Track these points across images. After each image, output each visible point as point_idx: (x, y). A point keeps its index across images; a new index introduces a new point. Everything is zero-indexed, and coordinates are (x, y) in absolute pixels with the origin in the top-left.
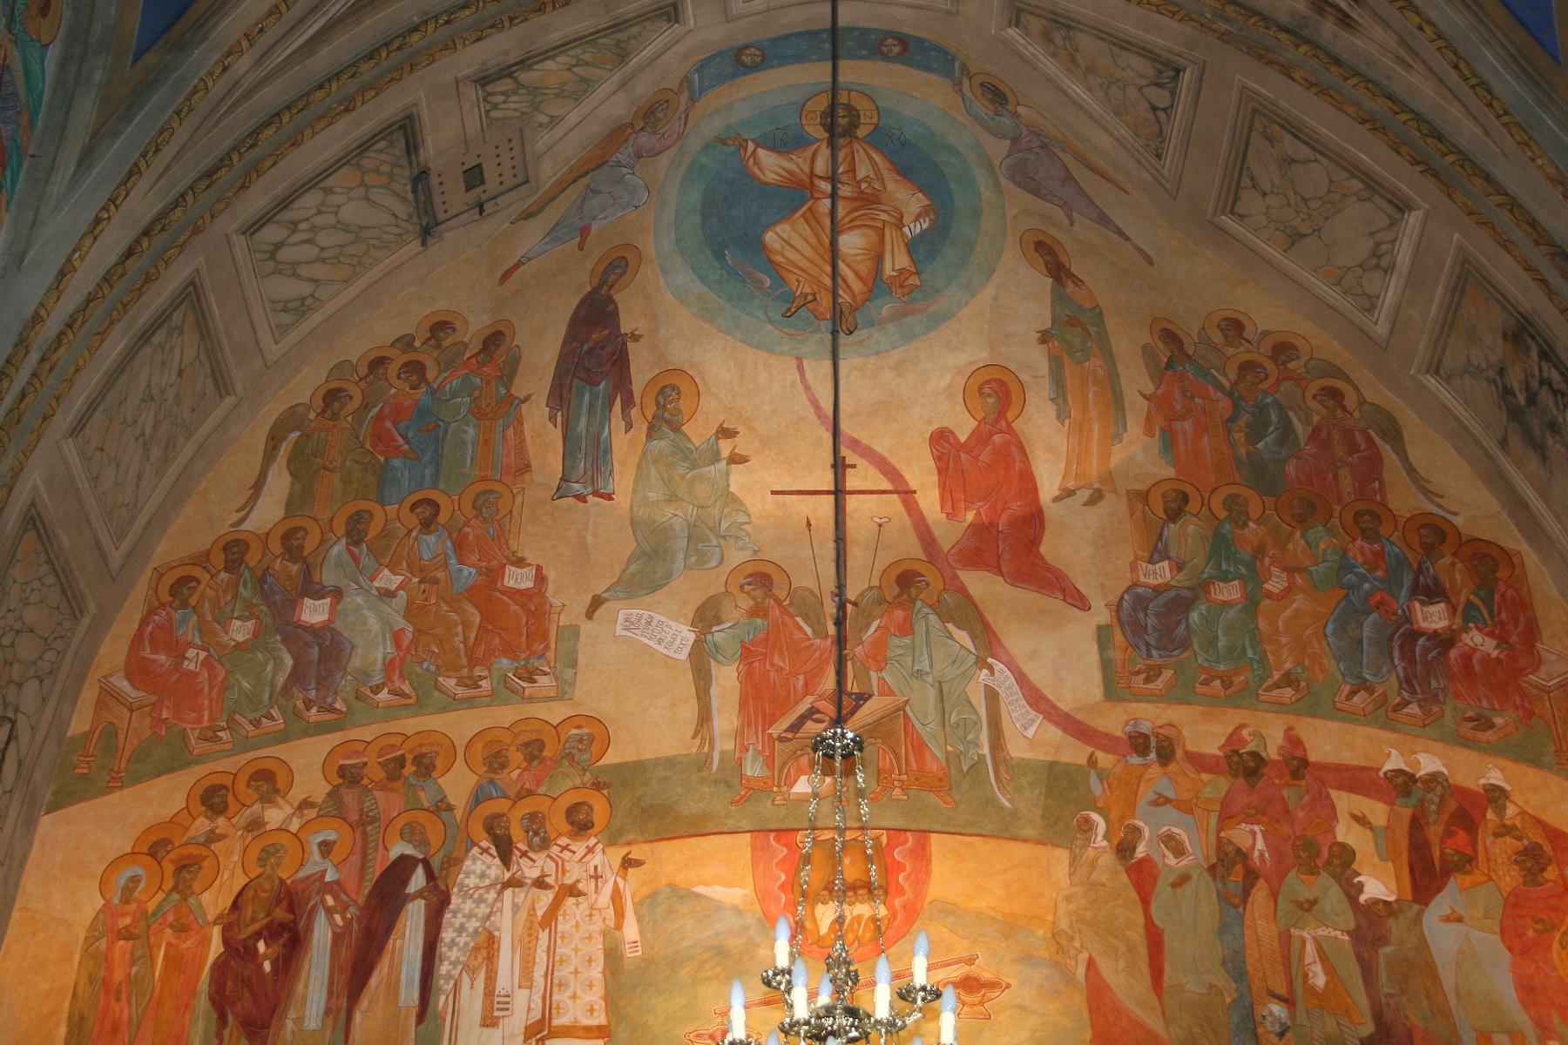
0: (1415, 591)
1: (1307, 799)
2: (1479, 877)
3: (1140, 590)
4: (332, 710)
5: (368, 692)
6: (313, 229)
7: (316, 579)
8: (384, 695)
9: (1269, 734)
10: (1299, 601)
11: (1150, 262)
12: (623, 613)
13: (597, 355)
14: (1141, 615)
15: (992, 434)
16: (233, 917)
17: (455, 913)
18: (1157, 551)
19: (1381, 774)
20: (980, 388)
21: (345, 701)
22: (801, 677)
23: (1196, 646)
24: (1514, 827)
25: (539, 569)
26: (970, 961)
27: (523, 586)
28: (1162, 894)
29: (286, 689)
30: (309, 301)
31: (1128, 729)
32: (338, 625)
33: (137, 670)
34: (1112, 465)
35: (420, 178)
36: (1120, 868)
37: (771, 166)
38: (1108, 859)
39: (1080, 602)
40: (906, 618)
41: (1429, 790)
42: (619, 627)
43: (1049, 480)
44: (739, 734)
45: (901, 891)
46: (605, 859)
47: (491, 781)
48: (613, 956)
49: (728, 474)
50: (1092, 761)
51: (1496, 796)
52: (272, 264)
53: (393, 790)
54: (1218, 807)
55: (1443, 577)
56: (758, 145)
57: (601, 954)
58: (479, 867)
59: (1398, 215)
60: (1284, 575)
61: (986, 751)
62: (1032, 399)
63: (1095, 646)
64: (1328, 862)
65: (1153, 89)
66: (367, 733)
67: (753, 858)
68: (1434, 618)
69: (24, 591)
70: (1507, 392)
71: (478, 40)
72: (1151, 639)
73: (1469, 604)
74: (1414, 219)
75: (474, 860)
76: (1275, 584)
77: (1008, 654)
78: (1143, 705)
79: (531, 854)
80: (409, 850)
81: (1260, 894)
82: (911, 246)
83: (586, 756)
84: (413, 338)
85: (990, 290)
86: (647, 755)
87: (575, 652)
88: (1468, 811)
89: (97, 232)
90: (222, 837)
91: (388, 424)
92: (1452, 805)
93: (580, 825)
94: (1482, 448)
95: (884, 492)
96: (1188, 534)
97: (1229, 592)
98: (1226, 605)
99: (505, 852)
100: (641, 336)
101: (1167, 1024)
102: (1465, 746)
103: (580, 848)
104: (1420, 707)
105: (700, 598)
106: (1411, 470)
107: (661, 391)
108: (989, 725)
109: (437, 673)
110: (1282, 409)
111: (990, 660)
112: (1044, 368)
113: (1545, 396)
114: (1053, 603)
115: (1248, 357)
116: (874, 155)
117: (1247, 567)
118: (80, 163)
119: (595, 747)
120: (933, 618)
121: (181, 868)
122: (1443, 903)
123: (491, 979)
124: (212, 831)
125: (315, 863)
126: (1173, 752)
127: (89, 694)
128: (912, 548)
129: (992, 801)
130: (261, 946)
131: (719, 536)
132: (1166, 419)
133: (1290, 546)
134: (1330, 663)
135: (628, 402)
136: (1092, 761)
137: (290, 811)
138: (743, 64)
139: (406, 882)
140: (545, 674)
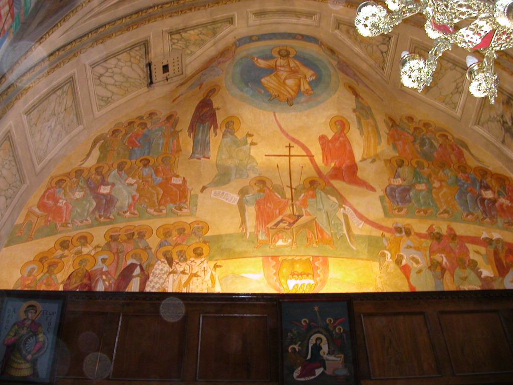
1: (458, 246)
4: (109, 218)
5: (122, 213)
6: (113, 72)
7: (106, 180)
8: (128, 214)
10: (445, 190)
12: (213, 192)
14: (394, 193)
15: (339, 137)
16: (68, 282)
17: (151, 282)
18: (396, 175)
20: (335, 123)
21: (114, 216)
25: (184, 178)
28: (413, 275)
29: (93, 212)
30: (110, 99)
31: (394, 226)
32: (113, 193)
33: (42, 205)
34: (378, 152)
37: (262, 63)
38: (393, 265)
40: (313, 193)
42: (212, 195)
43: (358, 154)
44: (256, 227)
45: (319, 276)
46: (209, 265)
47: (166, 241)
49: (250, 149)
52: (98, 81)
55: (489, 184)
56: (258, 58)
58: (160, 267)
60: (439, 183)
61: (345, 232)
63: (379, 202)
64: (469, 265)
65: (382, 46)
66: (121, 225)
68: (488, 195)
69: (3, 162)
70: (505, 123)
72: (398, 200)
75: (159, 265)
76: (436, 184)
79: (180, 263)
80: (134, 261)
81: (447, 275)
82: (310, 83)
85: (336, 96)
86: (222, 233)
87: (196, 202)
89: (41, 41)
90: (66, 256)
93: (198, 253)
96: (406, 171)
97: (422, 187)
98: (421, 190)
99: (170, 262)
100: (220, 108)
103: (198, 261)
106: (473, 155)
108: (346, 224)
109: (147, 207)
110: (429, 139)
111: (344, 206)
112: (355, 118)
114: (364, 189)
116: (295, 61)
118: (38, 25)
120: (323, 194)
121: (50, 266)
124: (63, 254)
125: (99, 265)
128: (314, 174)
129: (349, 247)
131: (246, 170)
132: (394, 139)
134: (458, 206)
135: (216, 127)
137: (91, 248)
139: (133, 272)
140: (186, 208)
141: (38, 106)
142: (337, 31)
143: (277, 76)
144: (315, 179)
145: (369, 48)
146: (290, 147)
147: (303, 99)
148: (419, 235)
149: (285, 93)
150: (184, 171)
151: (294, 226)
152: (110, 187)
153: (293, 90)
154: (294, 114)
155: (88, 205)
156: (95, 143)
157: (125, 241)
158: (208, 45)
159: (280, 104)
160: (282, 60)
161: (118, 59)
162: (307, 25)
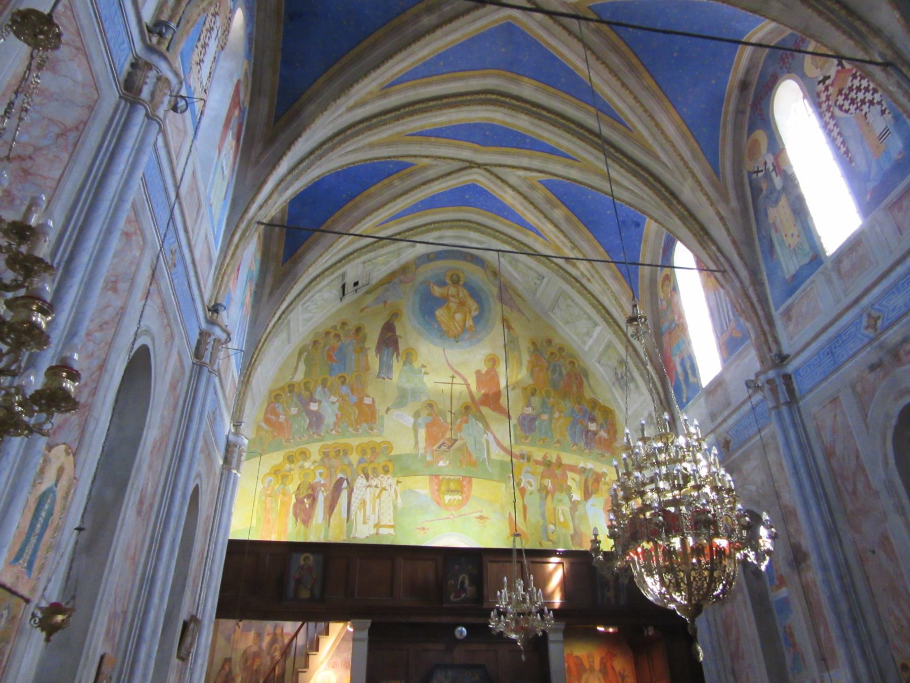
8: (334, 432)
10: (562, 420)
12: (394, 412)
13: (389, 340)
18: (529, 404)
28: (527, 496)
32: (321, 411)
37: (437, 291)
44: (425, 448)
46: (393, 481)
66: (330, 443)
74: (598, 329)
80: (342, 476)
93: (386, 472)
96: (536, 401)
97: (545, 417)
103: (386, 477)
122: (591, 501)
123: (365, 511)
128: (468, 400)
134: (568, 438)
143: (448, 308)
147: (467, 336)
148: (537, 462)
150: (377, 393)
156: (300, 354)
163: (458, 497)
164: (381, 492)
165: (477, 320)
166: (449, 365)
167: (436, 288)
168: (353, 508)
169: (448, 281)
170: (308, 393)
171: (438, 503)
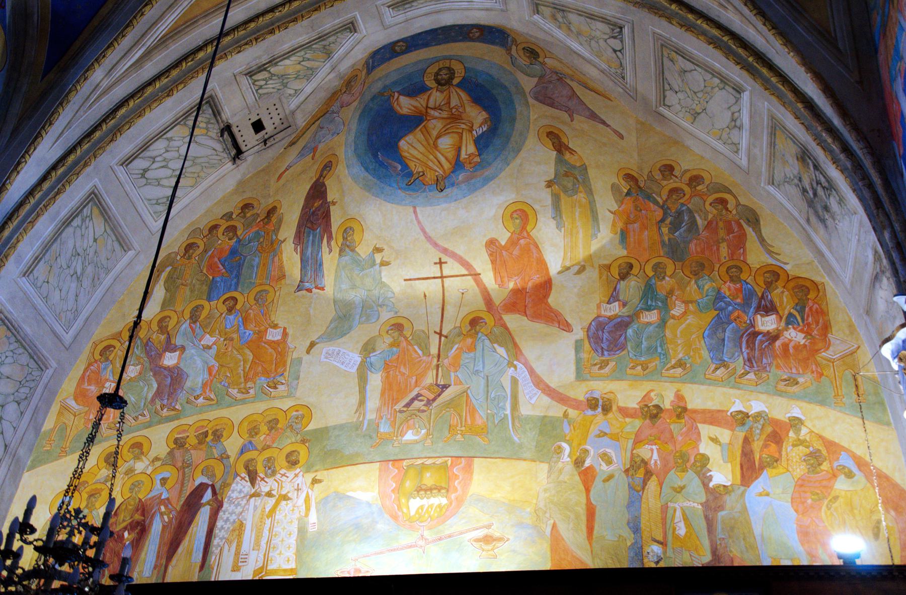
0: (758, 309)
2: (781, 470)
3: (601, 319)
4: (174, 409)
6: (165, 160)
7: (173, 342)
9: (665, 394)
10: (690, 319)
11: (621, 137)
13: (316, 216)
14: (600, 333)
15: (519, 239)
18: (613, 297)
19: (729, 414)
20: (511, 215)
21: (181, 404)
22: (414, 378)
23: (629, 348)
24: (805, 441)
25: (285, 329)
26: (489, 527)
27: (276, 339)
28: (597, 485)
31: (587, 396)
32: (182, 365)
34: (592, 251)
35: (227, 129)
36: (576, 473)
37: (405, 105)
39: (566, 327)
41: (756, 421)
42: (322, 357)
43: (554, 263)
44: (379, 410)
45: (456, 490)
46: (304, 479)
47: (250, 442)
48: (302, 531)
49: (380, 272)
50: (566, 415)
51: (796, 423)
52: (144, 180)
53: (201, 449)
54: (633, 437)
55: (777, 301)
57: (296, 530)
58: (239, 487)
59: (738, 96)
61: (508, 412)
62: (541, 218)
64: (694, 465)
66: (190, 421)
67: (380, 476)
70: (804, 191)
71: (239, 52)
72: (605, 346)
73: (790, 314)
74: (746, 96)
75: (238, 483)
76: (677, 311)
77: (526, 359)
78: (598, 382)
80: (205, 480)
81: (653, 484)
82: (477, 141)
83: (299, 426)
84: (232, 213)
88: (777, 434)
89: (19, 169)
91: (216, 259)
92: (769, 429)
93: (293, 462)
94: (799, 223)
95: (464, 275)
96: (631, 288)
97: (652, 317)
99: (253, 478)
101: (593, 558)
102: (780, 396)
103: (291, 474)
104: (755, 374)
105: (365, 339)
106: (762, 241)
107: (345, 231)
111: (515, 362)
112: (549, 201)
113: (820, 191)
114: (554, 330)
115: (675, 185)
117: (662, 302)
118: (12, 134)
119: (305, 421)
120: (487, 342)
122: (758, 485)
123: (239, 545)
126: (611, 407)
127: (55, 408)
128: (480, 304)
130: (126, 534)
133: (688, 288)
134: (705, 353)
136: (566, 415)
138: (395, 51)
139: (202, 497)
141: (44, 255)
142: (536, 17)
143: (426, 132)
144: (481, 315)
145: (593, 42)
146: (441, 263)
147: (461, 177)
148: (625, 412)
149: (435, 168)
150: (287, 317)
151: (435, 404)
152: (178, 353)
153: (447, 159)
154: (444, 205)
155: (146, 389)
157: (195, 448)
158: (321, 74)
159: (424, 191)
160: (438, 94)
161: (167, 139)
162: (487, 10)
163: (439, 500)
164: (277, 504)
165: (482, 143)
166: (429, 238)
167: (404, 100)
168: (215, 542)
169: (430, 82)
170: (163, 337)
171: (395, 517)
